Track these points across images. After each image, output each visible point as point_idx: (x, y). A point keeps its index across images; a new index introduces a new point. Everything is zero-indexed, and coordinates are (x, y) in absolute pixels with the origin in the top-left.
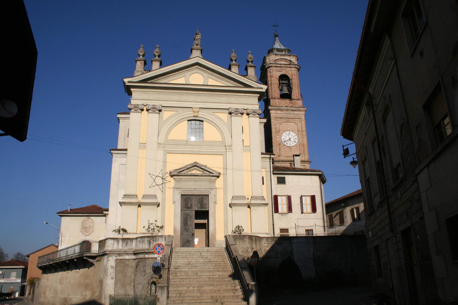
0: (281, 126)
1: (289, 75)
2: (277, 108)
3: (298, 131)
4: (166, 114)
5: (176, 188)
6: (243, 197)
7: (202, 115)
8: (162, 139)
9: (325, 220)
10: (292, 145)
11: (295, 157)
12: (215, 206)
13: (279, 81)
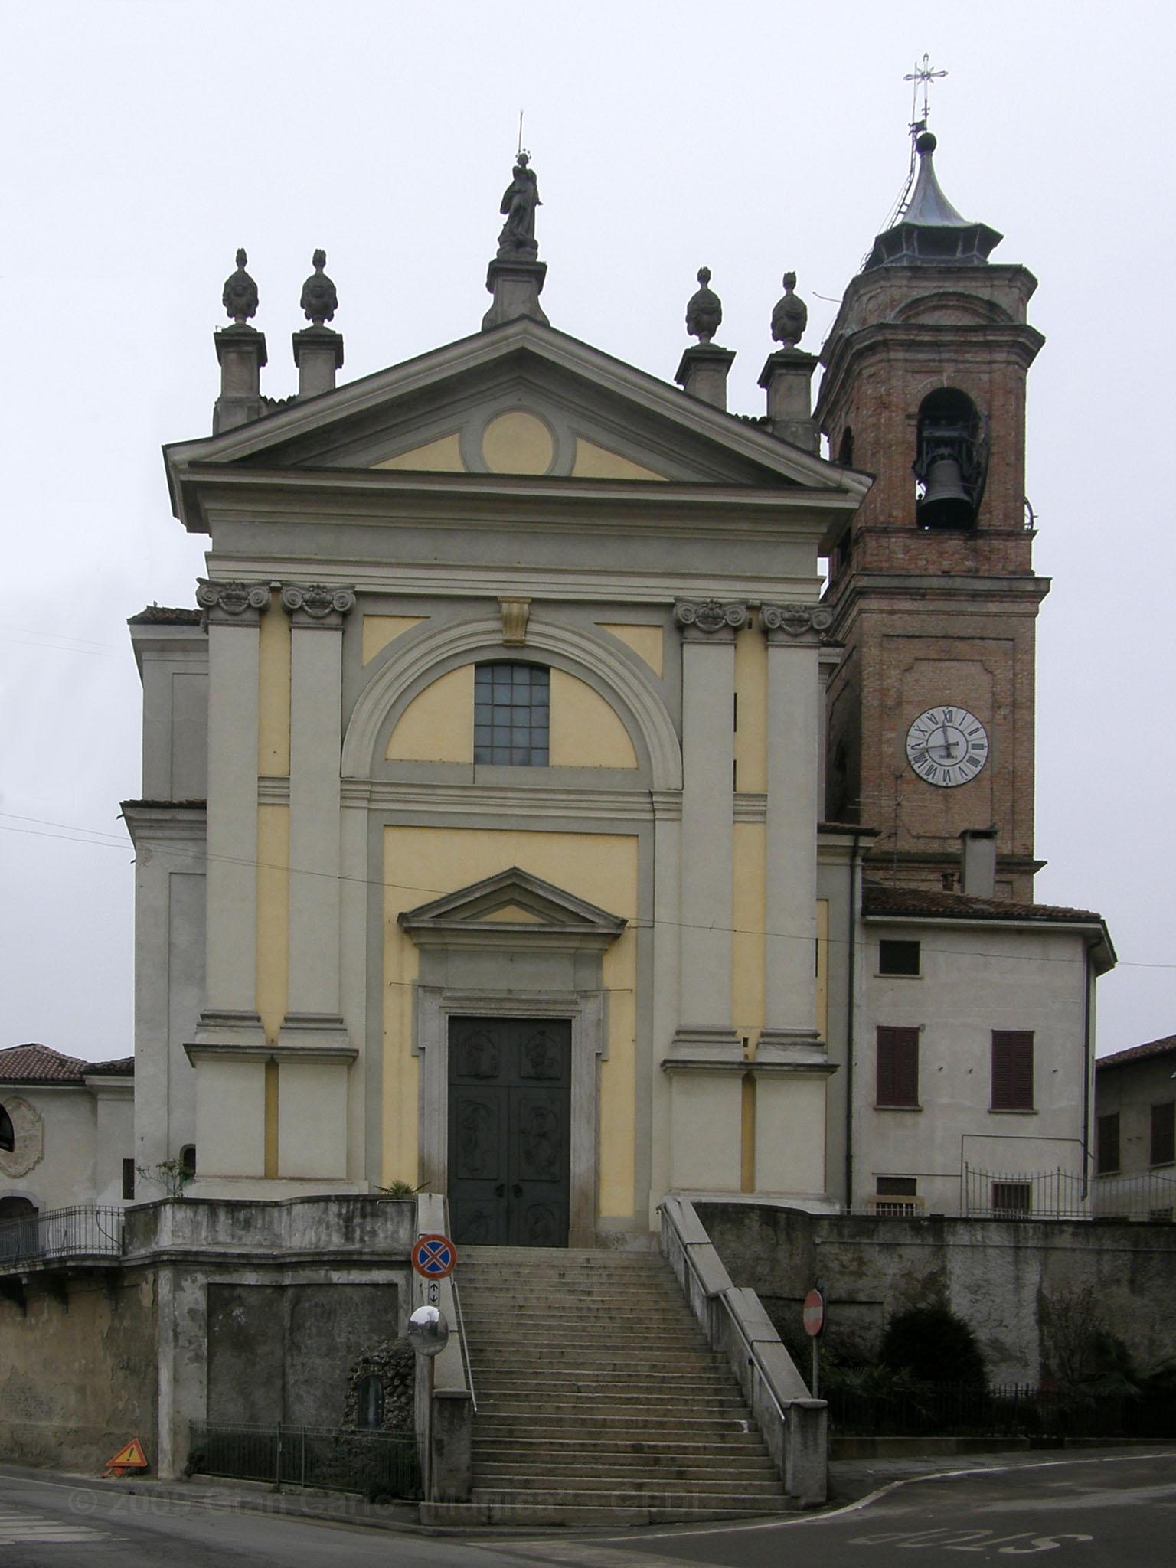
0: (909, 678)
1: (973, 395)
2: (896, 583)
3: (996, 706)
4: (379, 633)
5: (425, 989)
6: (725, 1035)
7: (547, 635)
8: (359, 764)
9: (1091, 1149)
10: (957, 778)
11: (969, 842)
12: (598, 1069)
13: (920, 428)
